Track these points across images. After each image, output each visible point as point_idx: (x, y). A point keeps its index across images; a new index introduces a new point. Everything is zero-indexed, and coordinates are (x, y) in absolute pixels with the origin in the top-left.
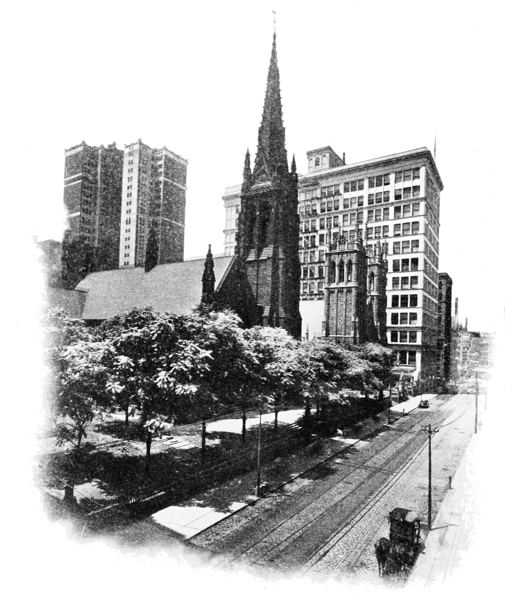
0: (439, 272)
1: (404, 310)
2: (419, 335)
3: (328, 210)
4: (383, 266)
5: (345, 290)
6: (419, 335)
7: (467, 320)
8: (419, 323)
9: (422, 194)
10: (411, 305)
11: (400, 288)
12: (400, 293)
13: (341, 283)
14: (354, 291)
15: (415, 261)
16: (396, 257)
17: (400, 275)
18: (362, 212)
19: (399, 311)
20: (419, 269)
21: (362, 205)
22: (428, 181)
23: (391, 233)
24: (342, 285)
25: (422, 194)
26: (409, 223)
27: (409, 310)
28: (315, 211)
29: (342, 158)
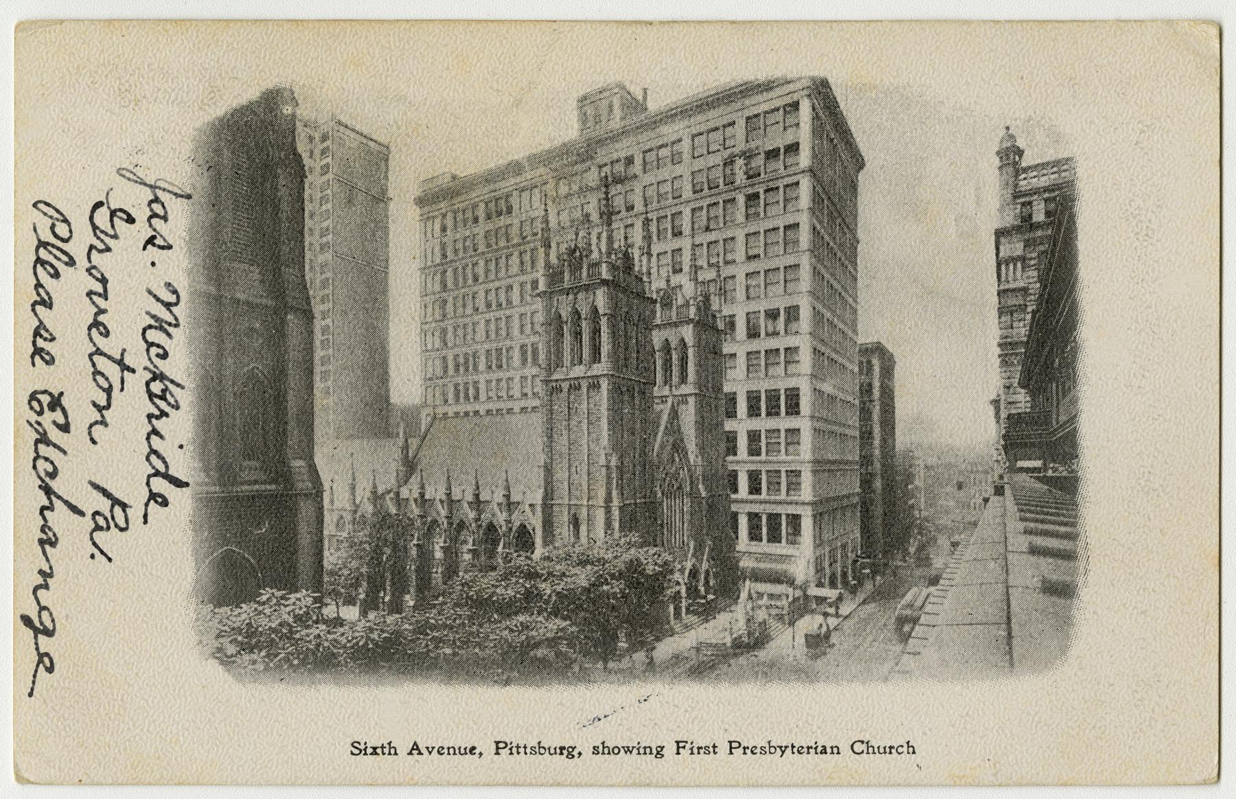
0: (861, 340)
1: (772, 423)
2: (807, 479)
3: (710, 188)
4: (711, 328)
5: (565, 386)
6: (807, 479)
7: (96, 487)
8: (806, 449)
9: (804, 159)
10: (787, 413)
11: (762, 375)
12: (763, 386)
13: (595, 366)
14: (604, 384)
15: (792, 313)
16: (752, 306)
17: (763, 344)
18: (797, 183)
19: (763, 424)
20: (738, 339)
21: (633, 208)
22: (817, 131)
23: (740, 254)
24: (579, 371)
25: (804, 159)
26: (776, 229)
27: (784, 423)
28: (588, 215)
29: (640, 98)
